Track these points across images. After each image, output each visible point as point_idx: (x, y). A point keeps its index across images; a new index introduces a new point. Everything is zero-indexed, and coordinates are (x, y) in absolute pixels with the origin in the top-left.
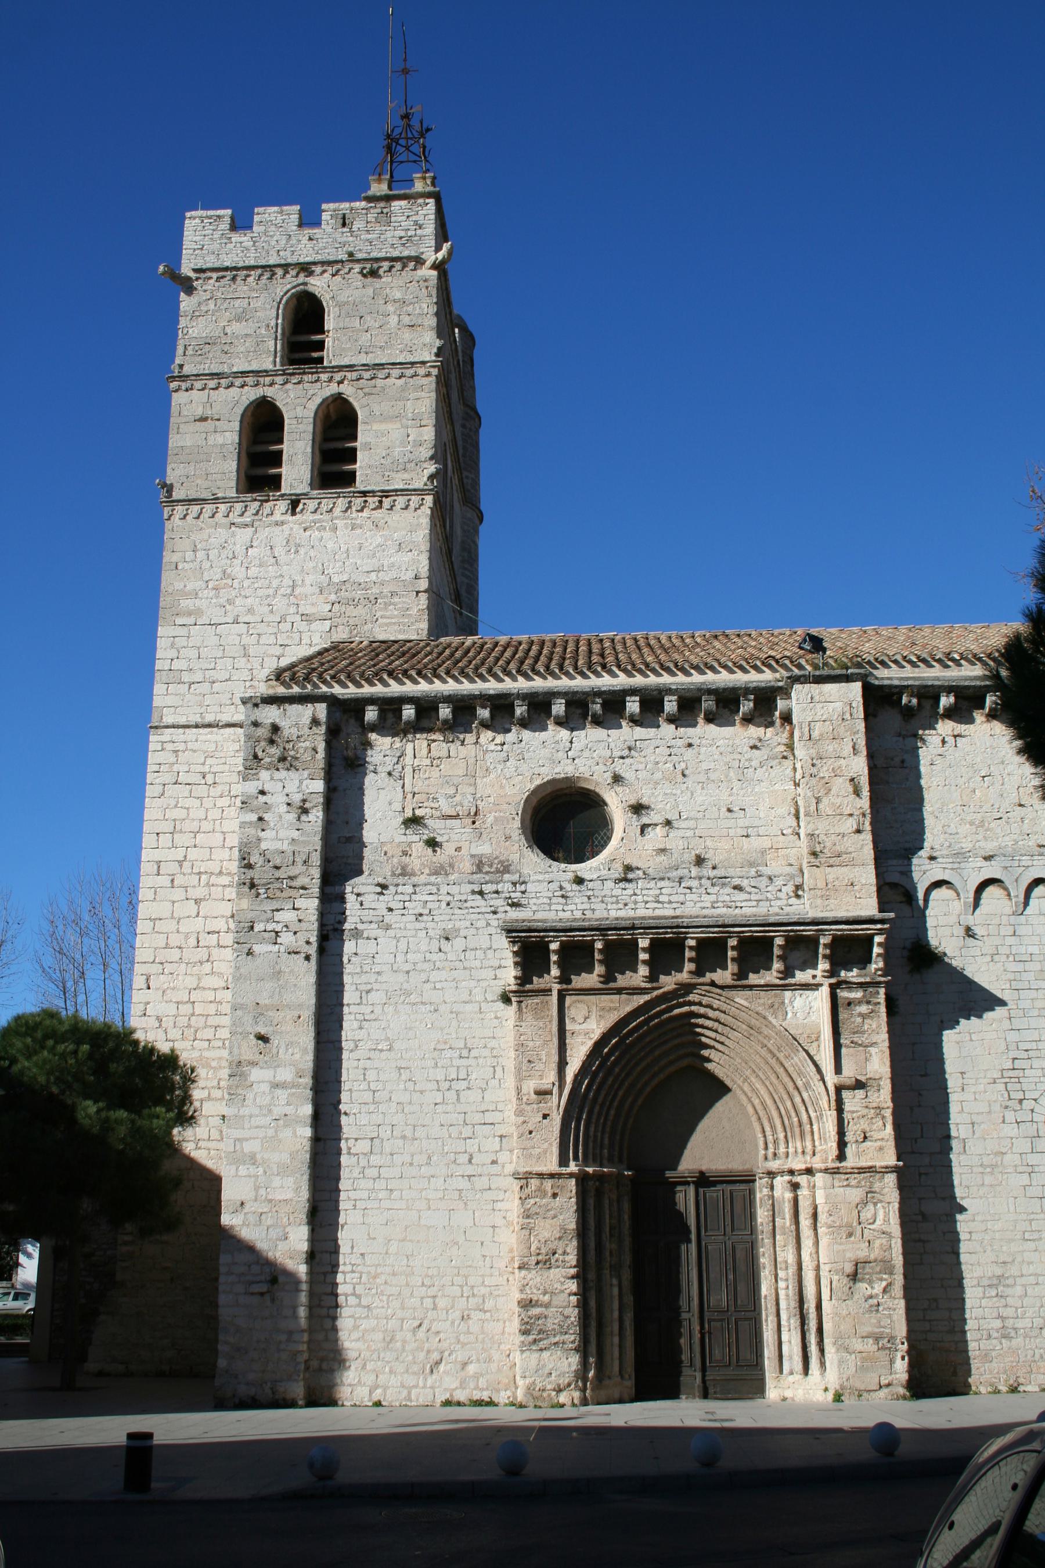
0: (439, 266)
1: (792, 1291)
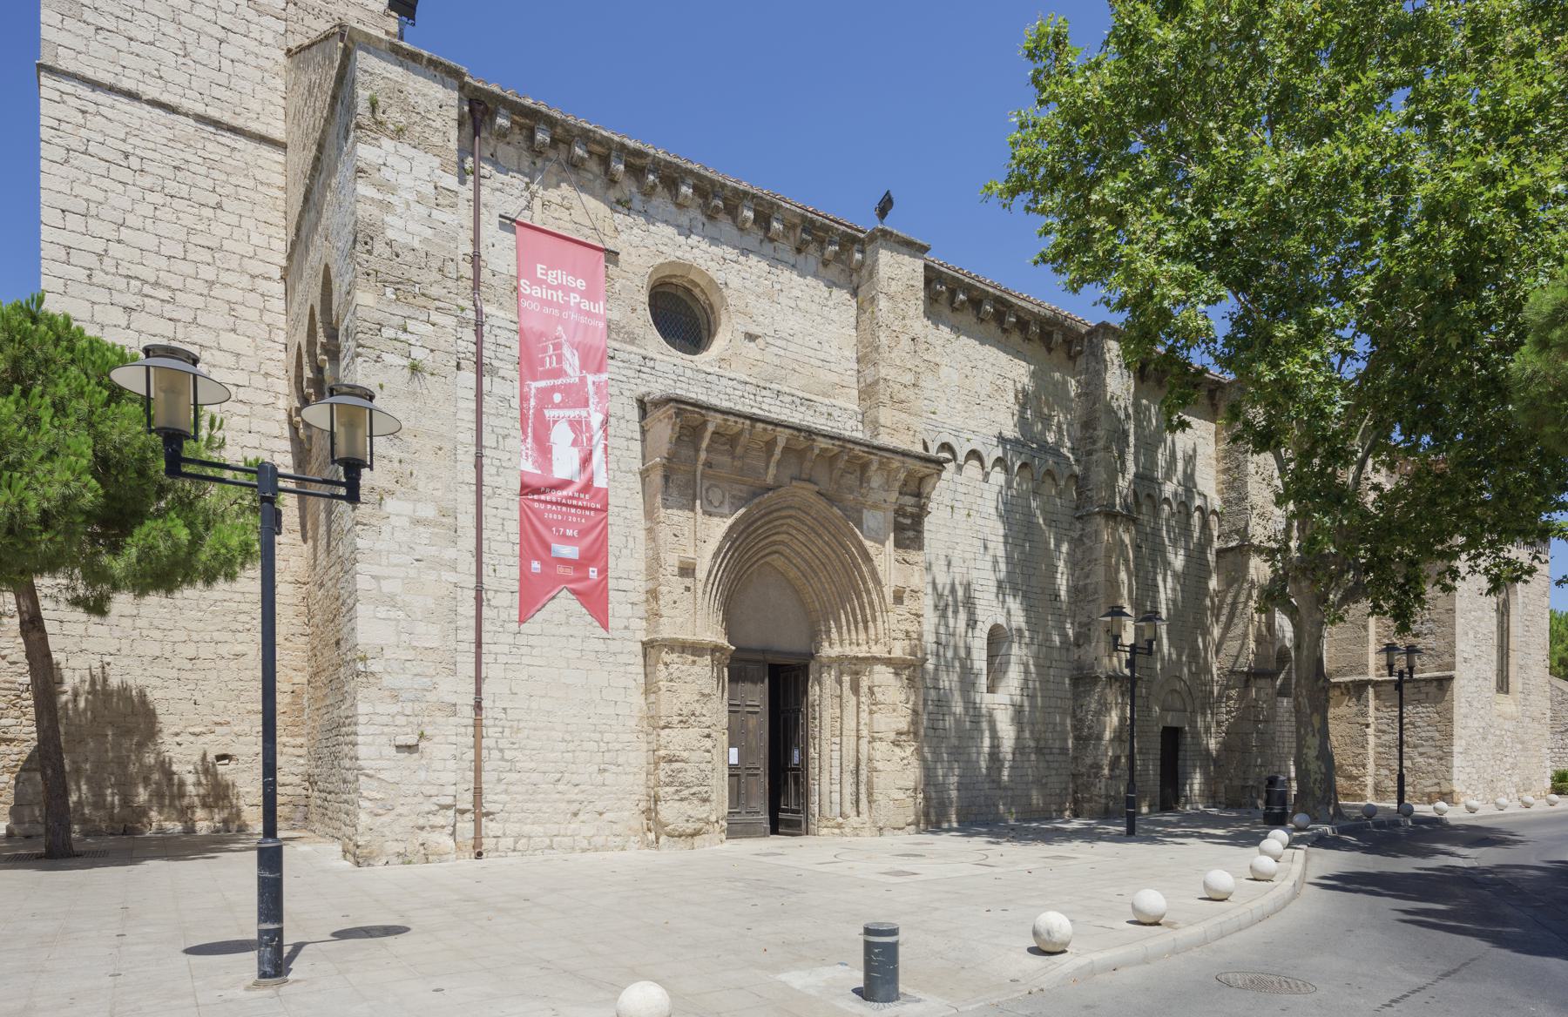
1: (853, 753)
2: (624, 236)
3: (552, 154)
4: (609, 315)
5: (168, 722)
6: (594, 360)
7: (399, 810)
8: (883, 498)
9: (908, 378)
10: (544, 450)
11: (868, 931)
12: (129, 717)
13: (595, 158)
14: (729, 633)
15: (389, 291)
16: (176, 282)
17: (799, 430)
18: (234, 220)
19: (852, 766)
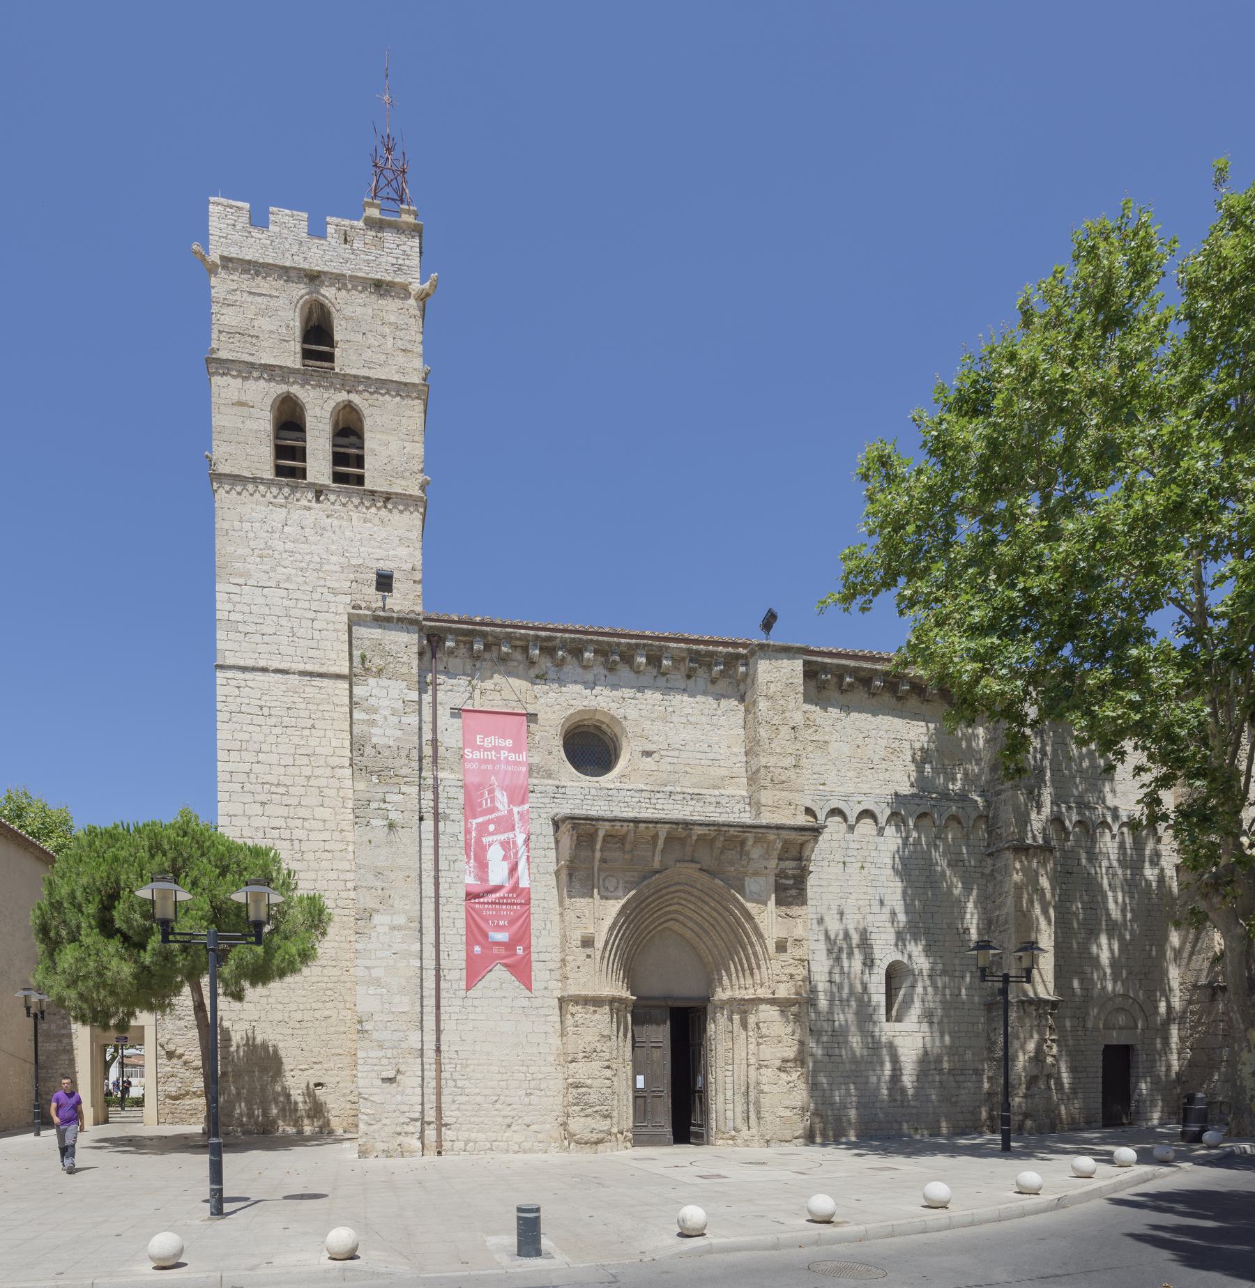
0: (423, 298)
1: (743, 1078)
2: (542, 701)
3: (487, 655)
4: (531, 760)
5: (288, 1064)
6: (519, 795)
7: (385, 1121)
8: (763, 866)
9: (789, 761)
10: (482, 866)
11: (520, 1210)
12: (266, 1061)
13: (519, 650)
14: (632, 988)
15: (375, 779)
16: (288, 781)
17: (677, 823)
18: (321, 733)
19: (743, 1089)
